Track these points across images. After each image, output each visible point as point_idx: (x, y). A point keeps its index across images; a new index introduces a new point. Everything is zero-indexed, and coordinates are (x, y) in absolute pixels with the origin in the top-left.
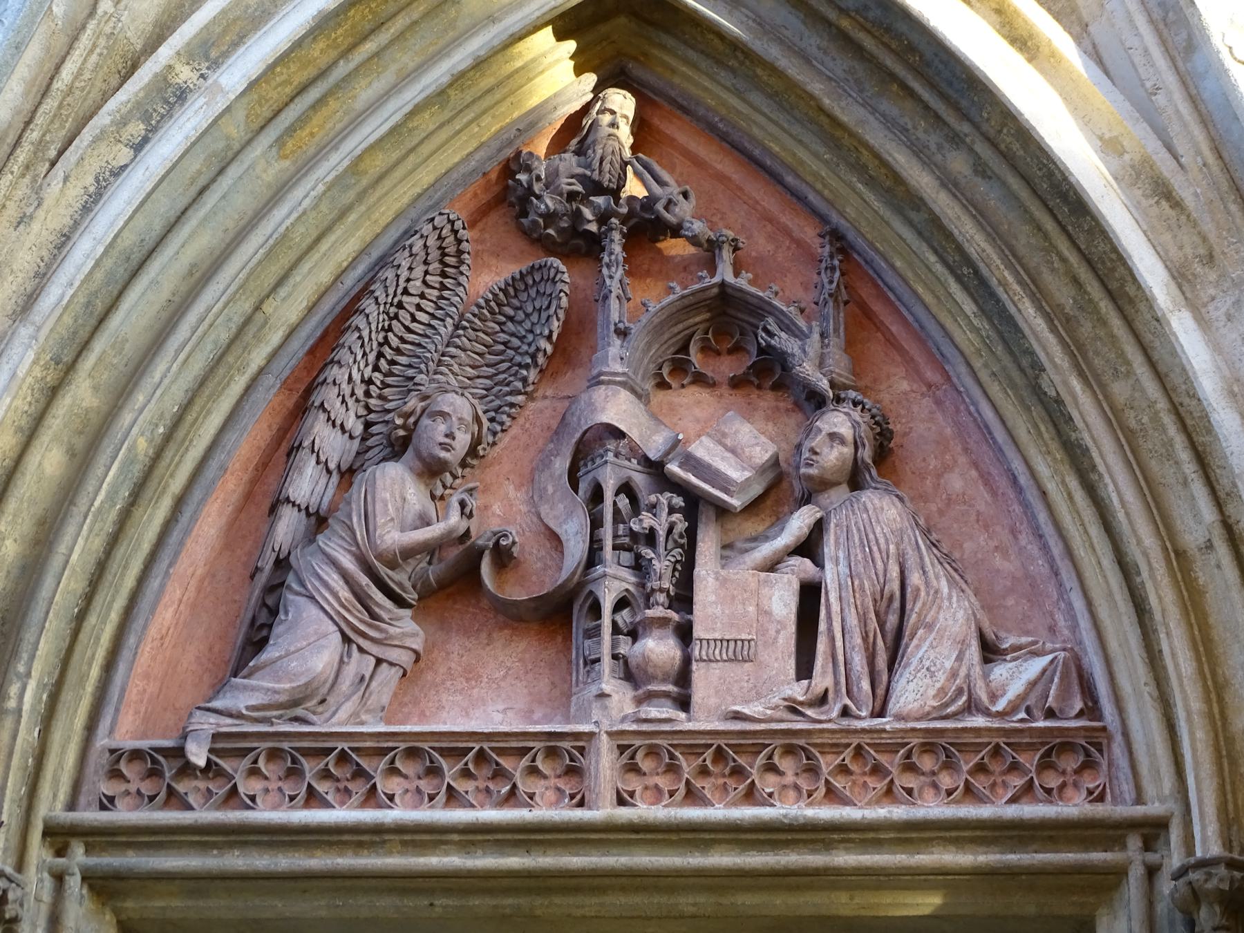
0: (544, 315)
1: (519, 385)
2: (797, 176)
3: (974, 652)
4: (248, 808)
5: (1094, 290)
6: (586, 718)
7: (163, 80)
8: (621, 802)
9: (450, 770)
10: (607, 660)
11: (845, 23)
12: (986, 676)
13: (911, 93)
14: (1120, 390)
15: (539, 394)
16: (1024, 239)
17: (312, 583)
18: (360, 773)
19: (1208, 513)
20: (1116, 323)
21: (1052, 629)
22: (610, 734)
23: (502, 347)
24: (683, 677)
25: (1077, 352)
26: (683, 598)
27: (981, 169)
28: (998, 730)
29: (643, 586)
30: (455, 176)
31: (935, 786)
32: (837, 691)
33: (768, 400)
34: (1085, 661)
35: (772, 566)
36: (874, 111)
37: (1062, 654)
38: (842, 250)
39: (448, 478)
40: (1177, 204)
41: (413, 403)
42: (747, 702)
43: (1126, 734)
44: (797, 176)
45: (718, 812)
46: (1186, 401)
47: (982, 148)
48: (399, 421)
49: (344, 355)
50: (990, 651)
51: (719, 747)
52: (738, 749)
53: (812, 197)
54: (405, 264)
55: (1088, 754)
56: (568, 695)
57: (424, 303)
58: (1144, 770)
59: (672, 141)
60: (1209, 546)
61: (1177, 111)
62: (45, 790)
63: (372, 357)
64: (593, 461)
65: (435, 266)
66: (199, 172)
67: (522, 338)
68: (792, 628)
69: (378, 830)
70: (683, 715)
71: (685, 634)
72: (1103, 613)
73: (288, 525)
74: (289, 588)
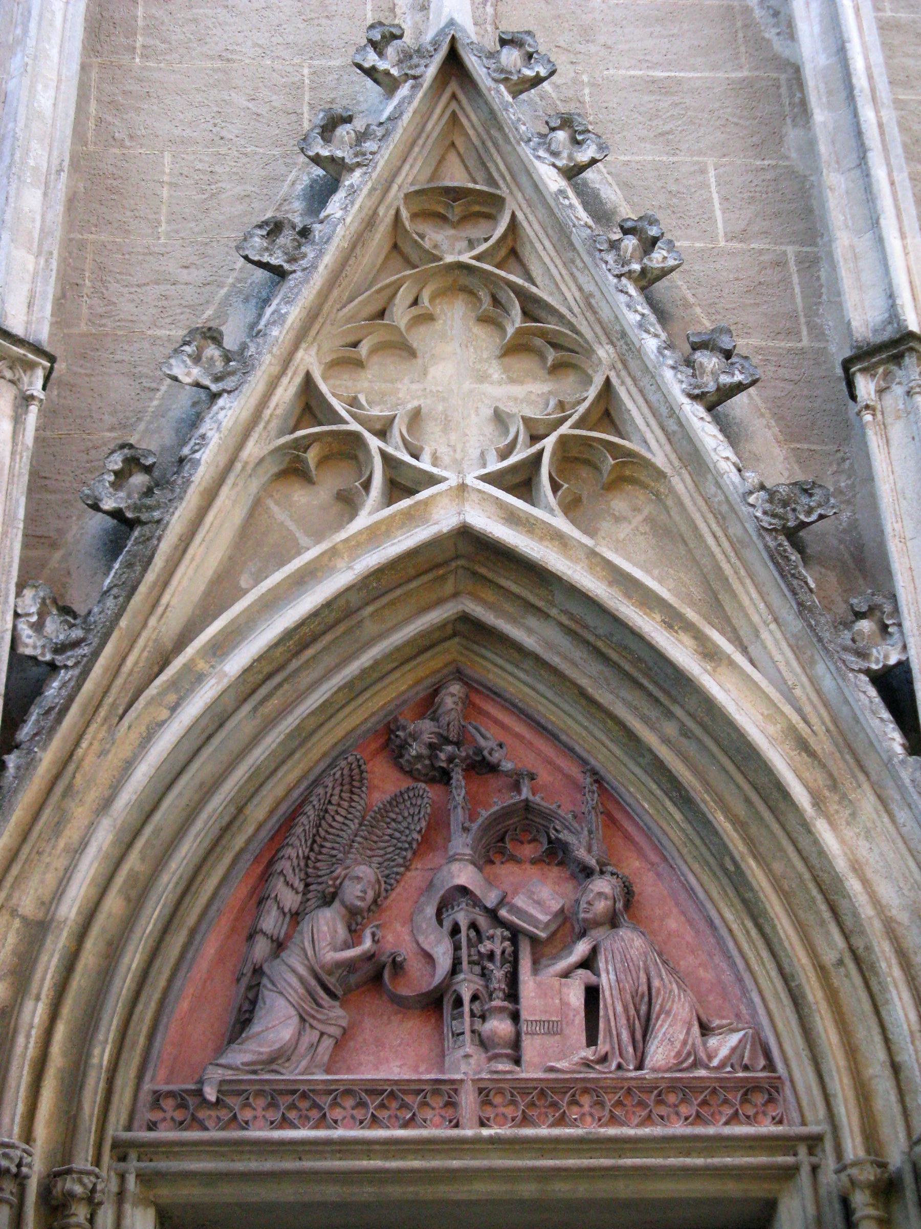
0: (416, 818)
1: (401, 861)
2: (568, 735)
3: (696, 1030)
4: (244, 1129)
6: (458, 1071)
7: (188, 667)
8: (482, 1124)
9: (373, 1103)
10: (468, 1036)
11: (599, 644)
12: (704, 1044)
13: (641, 686)
14: (778, 867)
15: (413, 867)
17: (281, 984)
18: (315, 1106)
20: (775, 827)
21: (738, 1016)
22: (473, 1080)
23: (387, 838)
24: (516, 1044)
25: (750, 842)
26: (513, 995)
27: (686, 733)
28: (716, 1078)
29: (487, 987)
30: (359, 732)
31: (677, 1114)
32: (614, 1053)
34: (762, 1035)
35: (566, 974)
36: (618, 697)
37: (751, 1031)
38: (596, 781)
39: (359, 919)
40: (812, 754)
42: (559, 1060)
43: (792, 1081)
44: (568, 735)
45: (544, 1131)
46: (821, 874)
48: (331, 883)
49: (293, 840)
50: (705, 1030)
51: (542, 1089)
52: (404, 1092)
53: (577, 748)
54: (330, 785)
55: (770, 1094)
56: (442, 1055)
57: (340, 810)
58: (805, 1103)
61: (809, 699)
62: (112, 1118)
63: (309, 843)
64: (453, 908)
65: (346, 787)
66: (207, 726)
67: (401, 832)
68: (583, 1014)
70: (518, 1069)
71: (515, 1017)
72: (772, 1005)
73: (261, 947)
74: (265, 986)
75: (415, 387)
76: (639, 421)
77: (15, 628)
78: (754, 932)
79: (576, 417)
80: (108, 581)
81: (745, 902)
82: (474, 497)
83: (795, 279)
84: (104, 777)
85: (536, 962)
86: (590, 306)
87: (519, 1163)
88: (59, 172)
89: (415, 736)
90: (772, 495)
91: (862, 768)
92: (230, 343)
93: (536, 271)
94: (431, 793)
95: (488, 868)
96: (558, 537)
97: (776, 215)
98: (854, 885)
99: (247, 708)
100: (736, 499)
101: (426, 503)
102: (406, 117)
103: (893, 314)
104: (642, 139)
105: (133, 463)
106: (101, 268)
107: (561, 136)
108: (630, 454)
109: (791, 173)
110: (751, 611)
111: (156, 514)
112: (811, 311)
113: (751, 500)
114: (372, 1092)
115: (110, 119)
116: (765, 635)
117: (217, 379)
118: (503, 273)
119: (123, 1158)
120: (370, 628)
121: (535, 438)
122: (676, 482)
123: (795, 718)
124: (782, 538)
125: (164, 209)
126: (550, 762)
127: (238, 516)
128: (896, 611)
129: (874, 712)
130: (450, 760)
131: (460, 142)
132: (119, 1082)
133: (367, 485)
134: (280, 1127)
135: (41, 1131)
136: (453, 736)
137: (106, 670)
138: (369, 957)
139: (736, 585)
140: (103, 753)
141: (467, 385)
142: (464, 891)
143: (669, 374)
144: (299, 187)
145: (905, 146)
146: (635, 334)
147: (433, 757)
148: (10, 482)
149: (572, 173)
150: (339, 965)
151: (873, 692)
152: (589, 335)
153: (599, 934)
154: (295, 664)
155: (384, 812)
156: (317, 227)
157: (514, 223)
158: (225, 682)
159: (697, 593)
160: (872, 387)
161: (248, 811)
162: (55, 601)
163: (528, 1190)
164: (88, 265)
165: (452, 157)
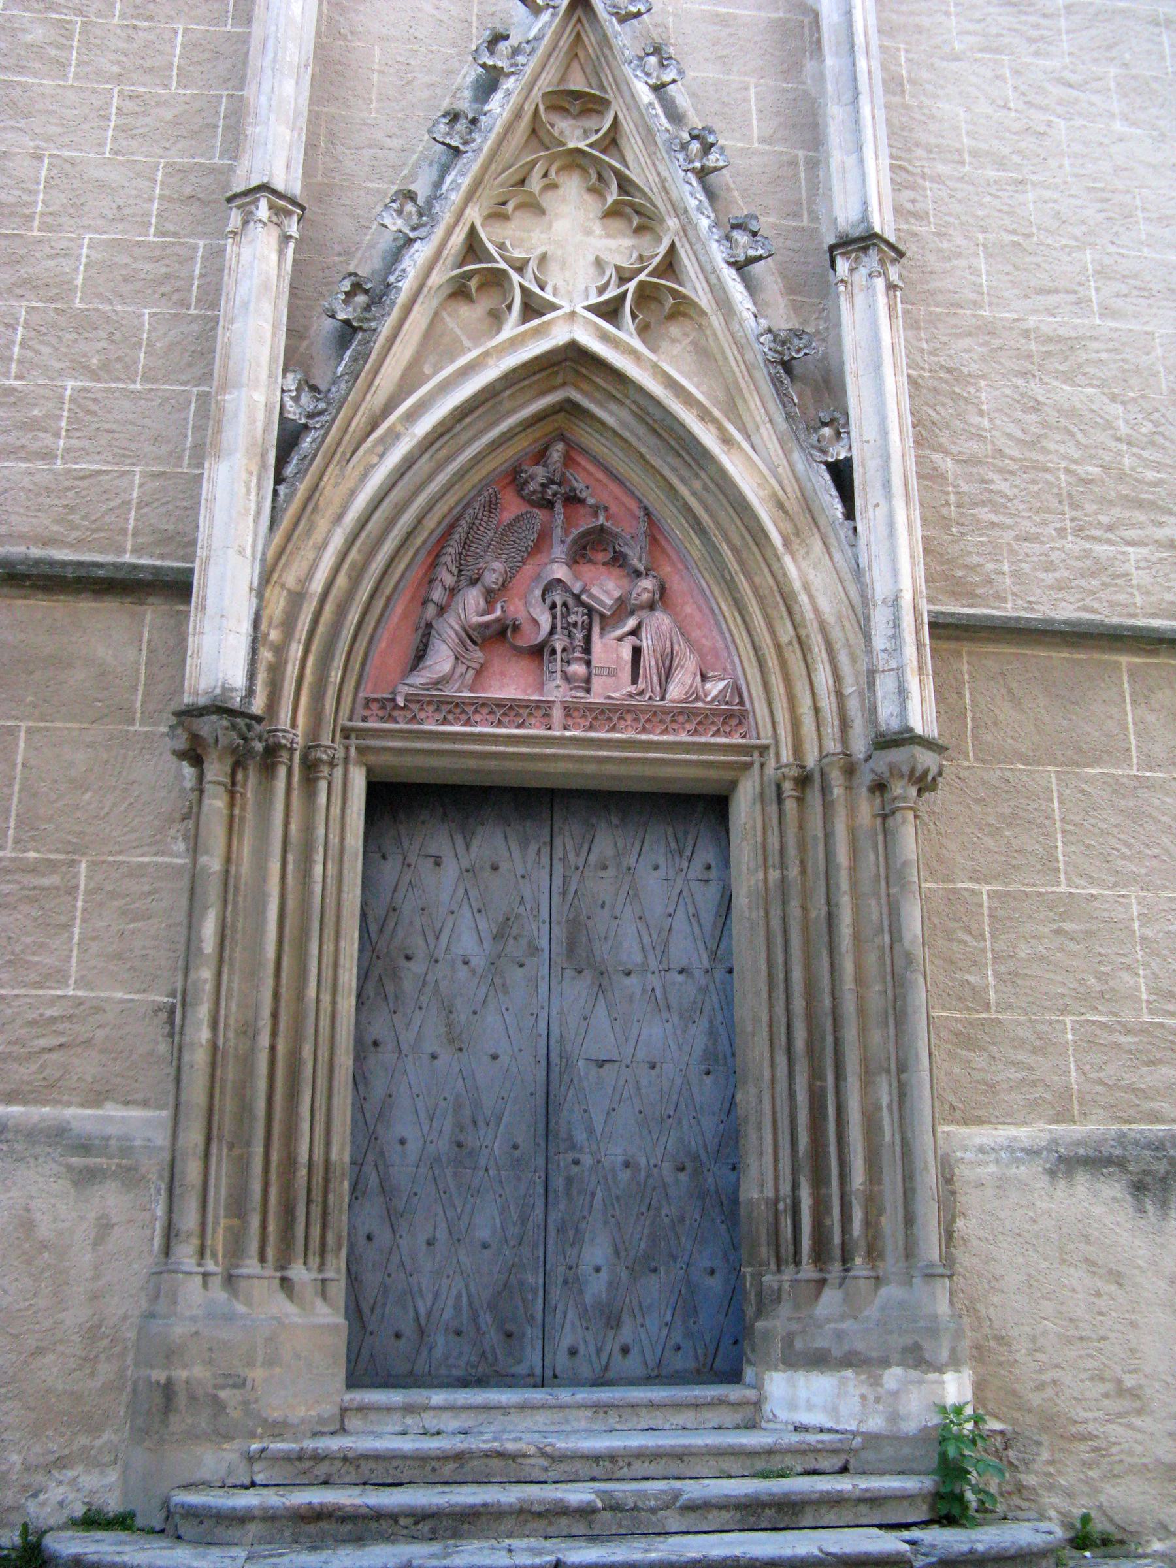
3: (699, 677)
7: (391, 429)
11: (656, 426)
13: (680, 456)
14: (757, 580)
21: (725, 670)
24: (588, 680)
25: (742, 563)
26: (587, 650)
33: (616, 571)
35: (620, 639)
40: (786, 512)
41: (482, 565)
45: (602, 735)
56: (542, 684)
59: (579, 464)
62: (341, 714)
71: (588, 663)
72: (746, 665)
73: (431, 610)
75: (543, 236)
78: (739, 619)
79: (650, 268)
80: (340, 369)
81: (735, 600)
82: (581, 320)
83: (802, 176)
84: (337, 501)
85: (602, 629)
86: (665, 188)
87: (587, 753)
88: (306, 66)
89: (532, 477)
90: (776, 336)
91: (816, 523)
92: (421, 201)
94: (540, 514)
95: (575, 567)
97: (794, 126)
98: (803, 598)
99: (427, 456)
100: (752, 339)
101: (548, 323)
102: (547, 38)
103: (865, 217)
104: (707, 60)
105: (357, 288)
106: (332, 133)
107: (653, 60)
108: (684, 297)
109: (806, 94)
110: (755, 413)
111: (373, 325)
112: (811, 200)
113: (762, 339)
114: (498, 705)
115: (337, 17)
116: (763, 430)
117: (414, 229)
118: (607, 159)
119: (347, 737)
120: (507, 405)
121: (623, 280)
122: (713, 319)
123: (777, 488)
124: (779, 367)
125: (375, 90)
126: (617, 498)
127: (424, 324)
128: (847, 423)
129: (827, 491)
130: (554, 495)
131: (581, 54)
132: (345, 692)
133: (509, 307)
134: (443, 724)
135: (301, 720)
136: (557, 479)
137: (339, 429)
138: (498, 620)
139: (747, 395)
140: (336, 485)
141: (579, 237)
142: (559, 581)
143: (715, 245)
144: (469, 80)
145: (884, 82)
146: (694, 215)
147: (543, 493)
148: (277, 297)
149: (658, 88)
151: (827, 477)
152: (662, 209)
153: (644, 614)
154: (458, 428)
155: (510, 526)
156: (483, 118)
157: (616, 122)
159: (721, 396)
161: (425, 522)
162: (307, 382)
163: (591, 768)
164: (323, 131)
165: (575, 65)
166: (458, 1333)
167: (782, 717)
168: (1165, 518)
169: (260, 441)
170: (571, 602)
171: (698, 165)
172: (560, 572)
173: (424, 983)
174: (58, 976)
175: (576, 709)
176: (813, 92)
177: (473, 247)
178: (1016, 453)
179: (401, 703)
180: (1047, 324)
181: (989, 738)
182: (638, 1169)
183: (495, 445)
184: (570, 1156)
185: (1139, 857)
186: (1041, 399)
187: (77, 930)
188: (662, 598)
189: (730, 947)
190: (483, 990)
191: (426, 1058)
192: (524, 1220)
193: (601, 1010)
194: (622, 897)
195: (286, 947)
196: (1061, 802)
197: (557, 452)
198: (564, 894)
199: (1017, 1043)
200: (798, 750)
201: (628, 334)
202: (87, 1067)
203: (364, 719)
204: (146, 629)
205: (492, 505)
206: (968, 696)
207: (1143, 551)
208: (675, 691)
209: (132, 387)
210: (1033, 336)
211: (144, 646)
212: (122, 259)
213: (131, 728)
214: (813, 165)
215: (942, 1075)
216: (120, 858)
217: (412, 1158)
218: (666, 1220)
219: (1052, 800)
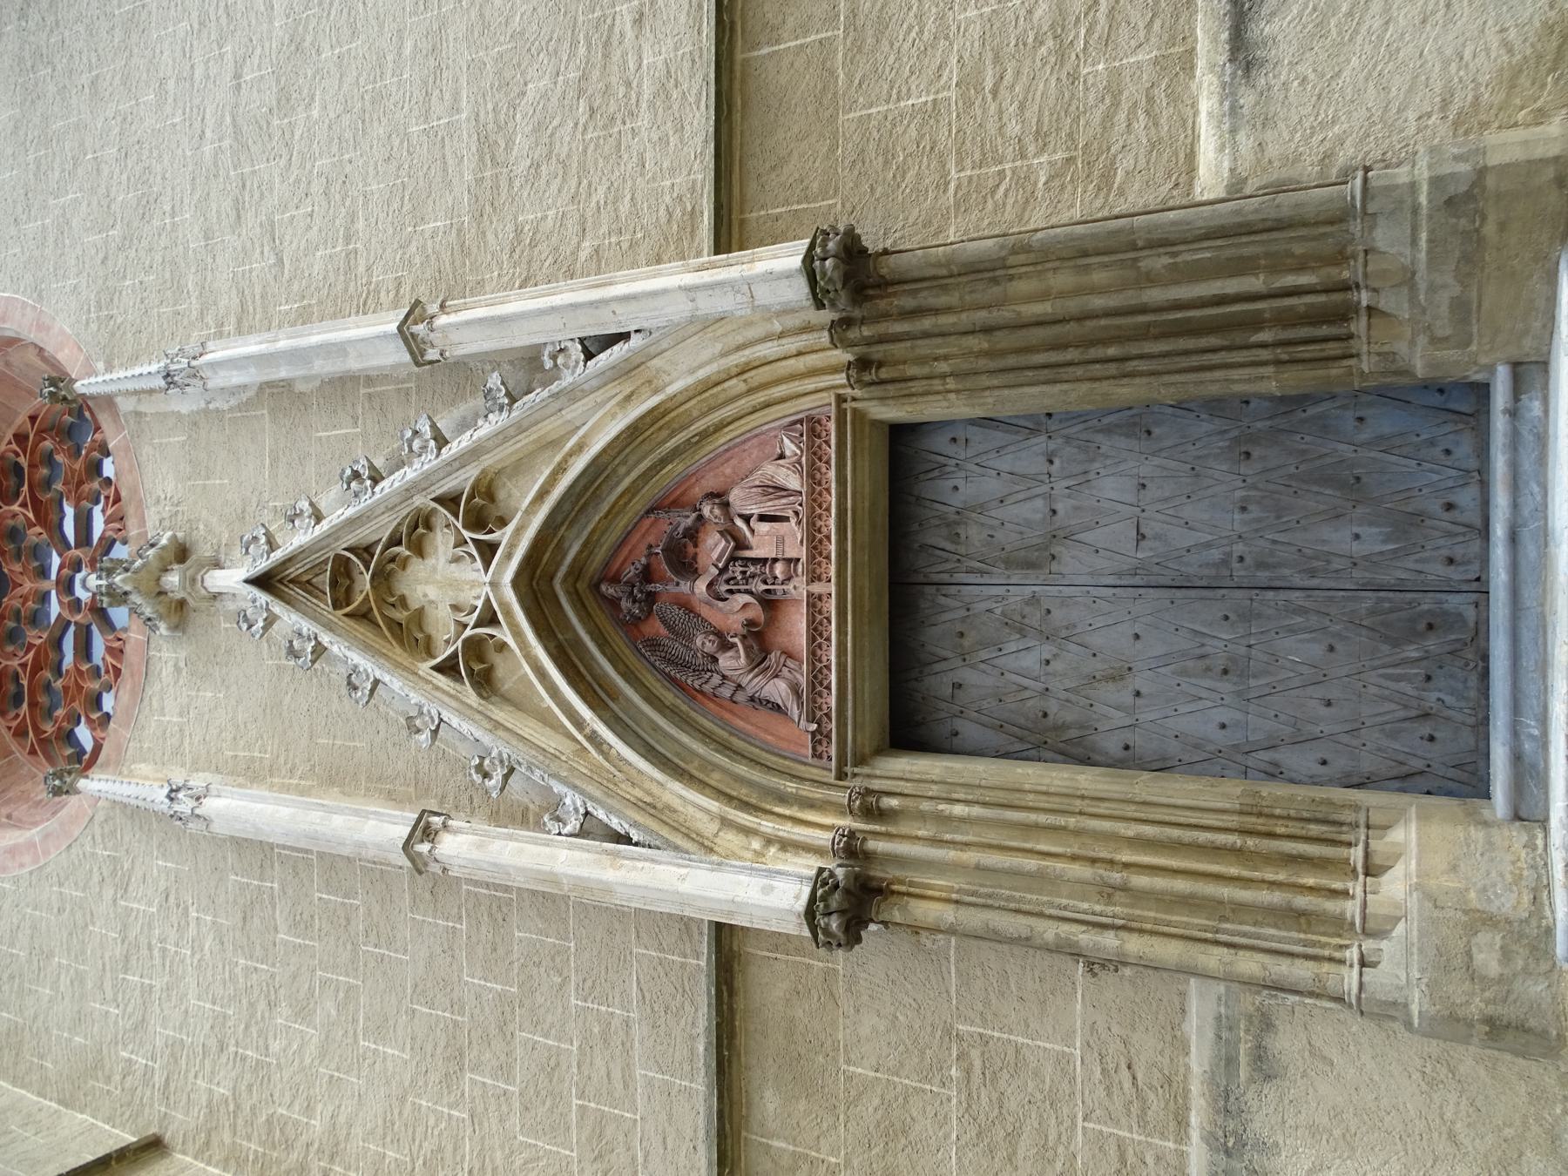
5: (662, 422)
6: (802, 594)
13: (600, 485)
14: (695, 413)
16: (646, 447)
19: (734, 381)
20: (673, 414)
21: (776, 437)
24: (789, 561)
27: (624, 462)
33: (701, 535)
35: (752, 531)
40: (632, 393)
45: (833, 547)
47: (616, 462)
50: (782, 456)
58: (820, 403)
60: (745, 381)
62: (825, 780)
69: (839, 664)
71: (775, 560)
72: (770, 418)
76: (454, 483)
77: (566, 835)
78: (731, 427)
81: (715, 431)
83: (378, 389)
86: (392, 508)
91: (638, 366)
93: (375, 538)
95: (700, 571)
96: (519, 531)
98: (702, 374)
104: (304, 473)
108: (473, 488)
114: (814, 640)
116: (569, 417)
122: (486, 464)
130: (641, 592)
131: (305, 578)
133: (492, 637)
138: (744, 637)
142: (710, 585)
150: (747, 656)
152: (409, 509)
154: (589, 678)
158: (596, 719)
160: (430, 351)
166: (1429, 678)
167: (810, 384)
168: (617, 30)
169: (597, 856)
170: (725, 577)
171: (368, 483)
172: (701, 586)
173: (1067, 701)
174: (1062, 1060)
175: (814, 572)
176: (318, 383)
177: (448, 668)
178: (574, 182)
179: (815, 726)
180: (469, 164)
181: (815, 185)
182: (1245, 499)
183: (602, 644)
184: (1236, 565)
185: (920, 17)
186: (528, 162)
187: (1020, 1040)
188: (719, 497)
189: (1024, 417)
190: (1072, 647)
191: (1139, 701)
192: (1302, 611)
193: (1087, 537)
194: (982, 519)
195: (1028, 845)
196: (871, 106)
197: (608, 590)
198: (982, 573)
199: (1108, 118)
200: (834, 370)
201: (503, 536)
202: (1147, 1047)
203: (830, 758)
204: (759, 952)
205: (654, 644)
206: (778, 210)
207: (646, 48)
208: (794, 482)
209: (573, 950)
210: (479, 175)
211: (774, 955)
212: (480, 951)
213: (841, 972)
214: (369, 380)
215: (1141, 202)
216: (953, 994)
217: (1238, 716)
218: (1302, 468)
219: (869, 115)
